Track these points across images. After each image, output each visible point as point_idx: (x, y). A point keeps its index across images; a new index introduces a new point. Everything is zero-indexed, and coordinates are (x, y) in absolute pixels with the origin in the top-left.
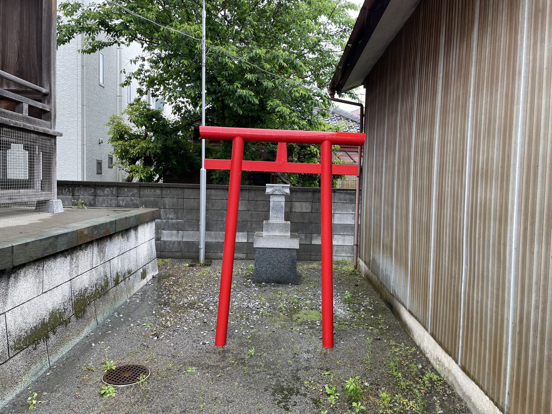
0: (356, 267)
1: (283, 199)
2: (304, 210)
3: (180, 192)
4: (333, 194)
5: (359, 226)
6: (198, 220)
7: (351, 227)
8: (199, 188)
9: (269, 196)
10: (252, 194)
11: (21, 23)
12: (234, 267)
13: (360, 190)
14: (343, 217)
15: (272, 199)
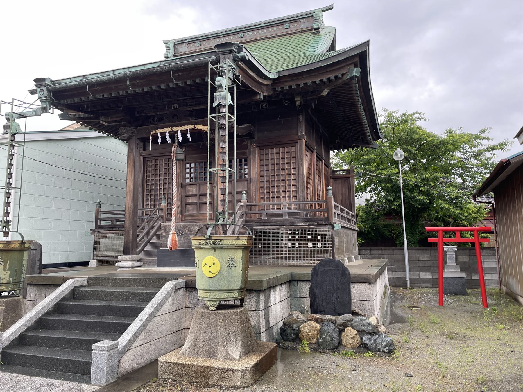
0: (501, 290)
1: (454, 253)
2: (465, 260)
3: (391, 251)
4: (481, 250)
5: (500, 269)
6: (405, 266)
7: (495, 269)
8: (403, 249)
9: (446, 252)
10: (432, 251)
11: (342, 190)
12: (482, 258)
13: (498, 248)
14: (489, 263)
15: (448, 253)
